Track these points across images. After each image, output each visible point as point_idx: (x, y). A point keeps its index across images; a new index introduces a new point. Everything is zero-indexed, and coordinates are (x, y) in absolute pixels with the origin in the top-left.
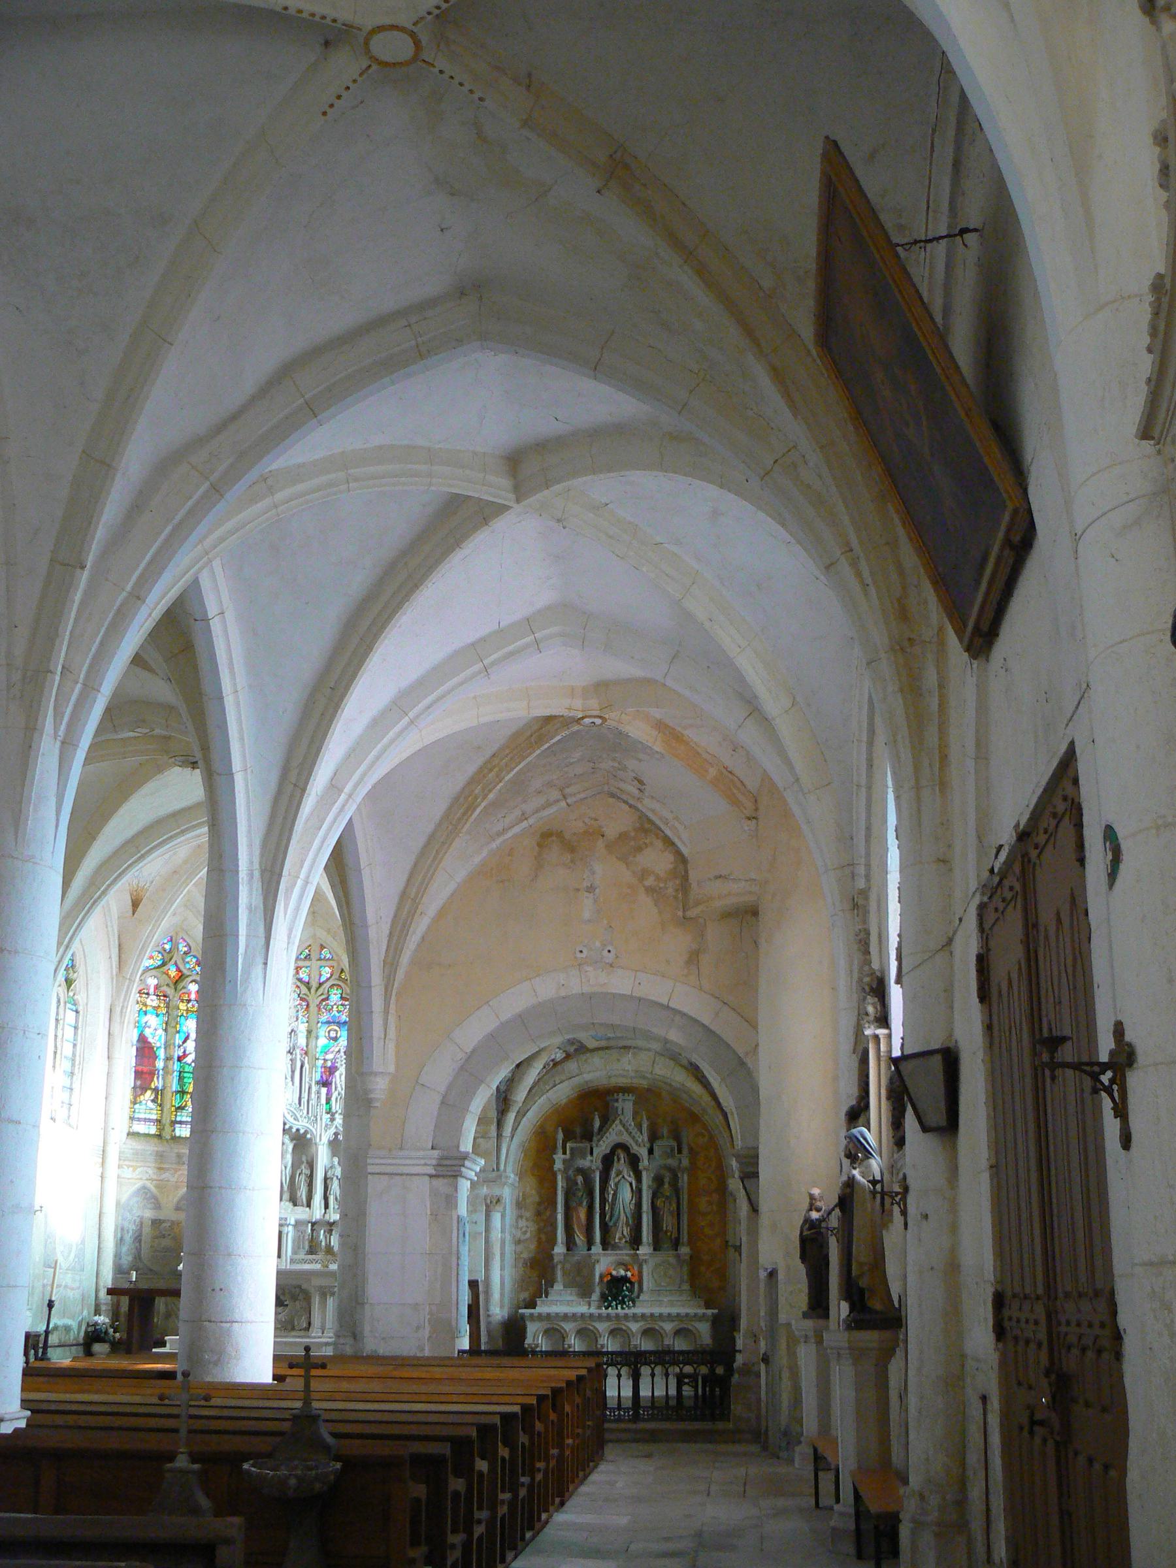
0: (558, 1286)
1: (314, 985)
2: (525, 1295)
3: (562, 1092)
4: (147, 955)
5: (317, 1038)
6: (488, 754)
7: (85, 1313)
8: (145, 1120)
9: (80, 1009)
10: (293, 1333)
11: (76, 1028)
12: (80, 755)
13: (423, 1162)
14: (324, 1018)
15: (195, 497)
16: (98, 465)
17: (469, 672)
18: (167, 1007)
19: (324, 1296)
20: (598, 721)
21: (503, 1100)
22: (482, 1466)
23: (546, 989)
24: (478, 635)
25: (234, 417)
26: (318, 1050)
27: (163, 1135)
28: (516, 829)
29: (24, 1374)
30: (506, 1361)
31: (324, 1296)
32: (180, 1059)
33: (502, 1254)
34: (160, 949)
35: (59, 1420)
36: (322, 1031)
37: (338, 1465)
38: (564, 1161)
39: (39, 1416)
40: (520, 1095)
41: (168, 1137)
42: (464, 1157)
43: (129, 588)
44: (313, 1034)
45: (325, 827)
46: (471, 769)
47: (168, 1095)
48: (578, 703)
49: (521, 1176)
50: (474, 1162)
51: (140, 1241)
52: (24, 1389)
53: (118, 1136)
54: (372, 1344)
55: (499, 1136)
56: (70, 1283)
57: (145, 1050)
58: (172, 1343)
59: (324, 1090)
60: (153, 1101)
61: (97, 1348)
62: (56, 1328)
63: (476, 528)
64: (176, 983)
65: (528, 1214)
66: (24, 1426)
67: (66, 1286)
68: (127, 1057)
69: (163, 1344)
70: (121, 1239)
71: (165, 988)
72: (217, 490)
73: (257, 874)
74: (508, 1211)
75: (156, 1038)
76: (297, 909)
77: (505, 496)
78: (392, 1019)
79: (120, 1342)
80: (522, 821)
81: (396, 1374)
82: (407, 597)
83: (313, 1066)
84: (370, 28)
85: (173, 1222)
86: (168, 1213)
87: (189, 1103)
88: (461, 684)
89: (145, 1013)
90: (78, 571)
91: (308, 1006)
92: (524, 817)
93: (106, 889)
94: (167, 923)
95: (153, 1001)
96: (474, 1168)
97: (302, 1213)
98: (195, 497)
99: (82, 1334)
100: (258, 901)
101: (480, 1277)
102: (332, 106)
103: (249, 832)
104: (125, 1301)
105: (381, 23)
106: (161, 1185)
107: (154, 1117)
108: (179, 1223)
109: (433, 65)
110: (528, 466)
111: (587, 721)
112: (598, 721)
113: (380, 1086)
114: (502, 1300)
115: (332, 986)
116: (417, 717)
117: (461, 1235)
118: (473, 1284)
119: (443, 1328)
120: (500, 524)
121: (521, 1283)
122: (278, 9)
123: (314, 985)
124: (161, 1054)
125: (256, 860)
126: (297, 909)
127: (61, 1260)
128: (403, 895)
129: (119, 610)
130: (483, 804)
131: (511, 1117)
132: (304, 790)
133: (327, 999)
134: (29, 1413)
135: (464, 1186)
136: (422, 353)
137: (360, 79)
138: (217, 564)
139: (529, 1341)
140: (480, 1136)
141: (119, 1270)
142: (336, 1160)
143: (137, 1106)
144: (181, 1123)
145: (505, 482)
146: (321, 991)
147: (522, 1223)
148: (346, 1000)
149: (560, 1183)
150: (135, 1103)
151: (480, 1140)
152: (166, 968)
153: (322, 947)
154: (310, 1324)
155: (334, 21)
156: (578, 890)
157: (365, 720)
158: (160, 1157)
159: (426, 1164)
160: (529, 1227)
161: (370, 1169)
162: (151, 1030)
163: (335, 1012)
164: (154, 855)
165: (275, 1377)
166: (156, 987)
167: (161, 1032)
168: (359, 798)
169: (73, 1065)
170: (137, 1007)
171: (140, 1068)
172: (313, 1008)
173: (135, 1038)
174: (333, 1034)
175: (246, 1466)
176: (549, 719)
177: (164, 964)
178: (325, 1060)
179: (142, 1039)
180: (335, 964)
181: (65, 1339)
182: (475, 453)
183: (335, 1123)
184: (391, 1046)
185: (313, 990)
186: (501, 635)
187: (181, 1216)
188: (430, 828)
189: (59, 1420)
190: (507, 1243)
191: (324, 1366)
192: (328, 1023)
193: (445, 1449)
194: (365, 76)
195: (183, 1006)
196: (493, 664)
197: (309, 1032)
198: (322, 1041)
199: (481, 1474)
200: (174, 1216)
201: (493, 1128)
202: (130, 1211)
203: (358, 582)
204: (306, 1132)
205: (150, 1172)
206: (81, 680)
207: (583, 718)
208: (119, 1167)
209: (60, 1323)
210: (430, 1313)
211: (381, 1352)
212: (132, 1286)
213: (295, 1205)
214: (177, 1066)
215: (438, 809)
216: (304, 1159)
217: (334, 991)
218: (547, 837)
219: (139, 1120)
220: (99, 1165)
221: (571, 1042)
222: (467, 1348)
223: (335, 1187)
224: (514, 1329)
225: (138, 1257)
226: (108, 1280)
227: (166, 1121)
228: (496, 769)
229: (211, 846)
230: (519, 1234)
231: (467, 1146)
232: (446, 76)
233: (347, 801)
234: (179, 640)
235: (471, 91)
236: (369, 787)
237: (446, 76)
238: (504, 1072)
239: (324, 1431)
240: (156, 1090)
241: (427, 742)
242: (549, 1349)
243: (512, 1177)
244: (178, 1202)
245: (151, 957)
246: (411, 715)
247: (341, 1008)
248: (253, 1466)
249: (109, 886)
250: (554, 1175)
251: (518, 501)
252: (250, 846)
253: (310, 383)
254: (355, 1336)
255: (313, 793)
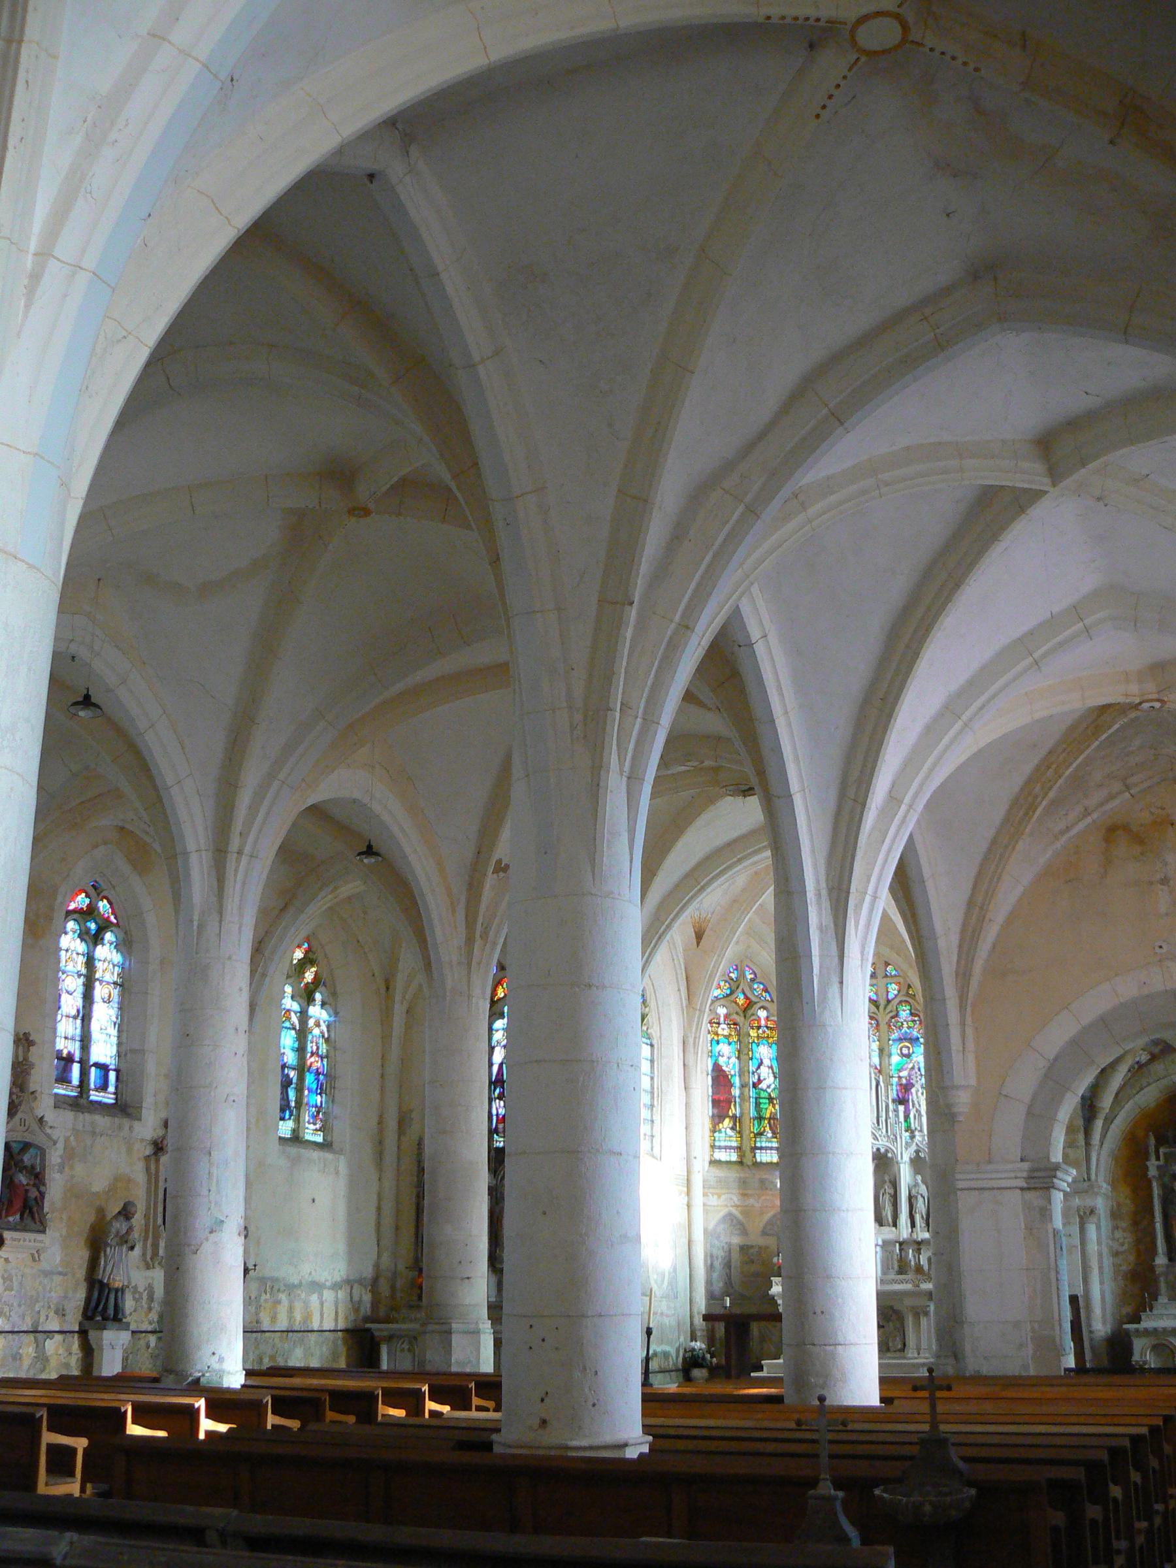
0: (1163, 1299)
1: (882, 1002)
2: (1127, 1310)
3: (1149, 1096)
4: (715, 984)
5: (890, 1055)
6: (1043, 752)
7: (682, 1339)
8: (726, 1148)
9: (655, 1042)
10: (889, 1355)
11: (652, 1061)
12: (647, 789)
13: (1013, 1175)
14: (895, 1036)
15: (731, 522)
16: (634, 502)
17: (1019, 668)
18: (739, 1035)
19: (917, 1316)
20: (1157, 705)
21: (1089, 1107)
22: (1116, 1491)
23: (1127, 988)
24: (1025, 629)
25: (762, 435)
26: (893, 1067)
27: (745, 1162)
28: (1081, 826)
29: (643, 1401)
30: (1118, 1379)
31: (917, 1316)
32: (755, 1085)
33: (1101, 1268)
34: (727, 978)
35: (680, 1445)
36: (895, 1049)
37: (973, 1492)
38: (1159, 1167)
39: (668, 1444)
40: (1106, 1102)
41: (750, 1163)
42: (1056, 1167)
43: (677, 618)
44: (886, 1052)
45: (888, 841)
46: (1028, 769)
47: (746, 1121)
48: (1134, 688)
49: (1113, 1184)
50: (1067, 1173)
51: (730, 1267)
52: (645, 1414)
53: (701, 1166)
54: (973, 1364)
55: (1088, 1144)
56: (666, 1312)
57: (720, 1078)
58: (771, 1367)
59: (901, 1108)
60: (732, 1129)
61: (697, 1373)
62: (655, 1354)
63: (1013, 519)
64: (745, 1011)
65: (1124, 1225)
66: (647, 1451)
67: (662, 1314)
68: (703, 1087)
69: (760, 1368)
70: (712, 1265)
71: (735, 1016)
72: (753, 512)
73: (824, 893)
74: (1103, 1223)
75: (730, 1065)
76: (868, 925)
77: (1041, 482)
78: (969, 1031)
79: (718, 1367)
80: (1085, 816)
81: (1004, 1394)
82: (948, 599)
83: (888, 1084)
84: (854, 20)
85: (760, 1248)
86: (756, 1239)
87: (768, 1129)
88: (1014, 679)
89: (718, 1042)
90: (627, 608)
91: (878, 1025)
92: (1087, 812)
93: (670, 923)
94: (731, 952)
95: (723, 1030)
96: (1066, 1178)
97: (889, 1233)
98: (731, 522)
99: (680, 1359)
100: (828, 920)
101: (1080, 1291)
102: (824, 107)
103: (813, 851)
104: (720, 1328)
105: (864, 11)
106: (746, 1211)
107: (734, 1144)
108: (767, 1247)
109: (922, 45)
110: (1060, 447)
111: (1146, 706)
112: (1157, 705)
113: (962, 1100)
114: (1104, 1316)
115: (900, 1002)
116: (971, 720)
117: (1058, 1250)
118: (1074, 1300)
119: (1047, 1346)
120: (1038, 511)
121: (1123, 1297)
122: (761, 20)
123: (882, 1002)
124: (736, 1081)
125: (823, 878)
126: (868, 925)
127: (655, 1288)
128: (970, 904)
129: (669, 642)
130: (1044, 803)
131: (1099, 1124)
132: (864, 805)
133: (897, 1015)
134: (650, 1438)
135: (1058, 1197)
136: (941, 345)
137: (849, 74)
138: (755, 589)
139: (1136, 1357)
140: (1070, 1144)
141: (711, 1296)
142: (919, 1178)
143: (716, 1134)
144: (761, 1148)
145: (1039, 467)
146: (889, 1008)
147: (1119, 1234)
148: (917, 1015)
149: (1156, 1191)
150: (714, 1131)
151: (1069, 1151)
152: (734, 996)
153: (887, 964)
154: (904, 1345)
155: (818, 20)
156: (1151, 883)
157: (918, 727)
158: (743, 1183)
159: (1016, 1178)
160: (1126, 1239)
161: (960, 1185)
162: (725, 1059)
163: (905, 1029)
164: (715, 884)
165: (882, 1400)
166: (726, 1017)
167: (734, 1060)
168: (920, 806)
169: (652, 1098)
170: (709, 1037)
171: (717, 1097)
172: (883, 1027)
173: (710, 1068)
174: (905, 1051)
175: (877, 1492)
176: (1104, 709)
177: (732, 993)
178: (900, 1078)
179: (717, 1068)
180: (901, 980)
181: (664, 1365)
182: (1004, 442)
183: (916, 1140)
184: (971, 1058)
185: (881, 1008)
186: (1052, 624)
187: (771, 1242)
188: (991, 833)
189: (680, 1445)
190: (1104, 1254)
191: (949, 1388)
192: (900, 1040)
193: (1079, 1474)
194: (855, 69)
195: (753, 1033)
196: (1044, 656)
197: (881, 1050)
198: (895, 1059)
199: (1115, 1500)
200: (761, 1241)
201: (1081, 1137)
202: (718, 1238)
203: (897, 588)
204: (887, 1151)
205: (735, 1199)
206: (640, 714)
207: (1140, 703)
208: (705, 1195)
209: (659, 1349)
210: (1033, 1330)
211: (985, 1371)
212: (727, 1312)
213: (881, 1225)
214: (753, 1093)
215: (998, 814)
216: (887, 1178)
217: (901, 1008)
218: (1113, 831)
219: (720, 1148)
220: (684, 1195)
221: (1156, 1042)
222: (1073, 1366)
223: (921, 1206)
224: (1118, 1348)
225: (729, 1283)
226: (701, 1305)
227: (746, 1148)
228: (1054, 766)
229: (776, 870)
230: (1116, 1246)
231: (1057, 1156)
232: (937, 54)
233: (908, 811)
234: (727, 670)
235: (965, 64)
236: (928, 795)
237: (937, 54)
238: (1088, 1079)
239: (954, 1455)
240: (734, 1117)
241: (982, 744)
242: (1159, 1366)
243: (1105, 1187)
244: (765, 1228)
245: (719, 986)
246: (964, 718)
247: (911, 1024)
248: (885, 1491)
249: (673, 920)
250: (1149, 1182)
251: (1054, 485)
252: (815, 866)
253: (830, 394)
254: (956, 1357)
255: (873, 807)
